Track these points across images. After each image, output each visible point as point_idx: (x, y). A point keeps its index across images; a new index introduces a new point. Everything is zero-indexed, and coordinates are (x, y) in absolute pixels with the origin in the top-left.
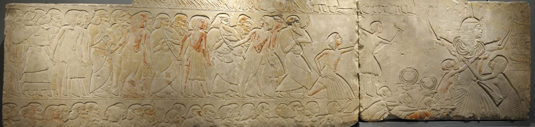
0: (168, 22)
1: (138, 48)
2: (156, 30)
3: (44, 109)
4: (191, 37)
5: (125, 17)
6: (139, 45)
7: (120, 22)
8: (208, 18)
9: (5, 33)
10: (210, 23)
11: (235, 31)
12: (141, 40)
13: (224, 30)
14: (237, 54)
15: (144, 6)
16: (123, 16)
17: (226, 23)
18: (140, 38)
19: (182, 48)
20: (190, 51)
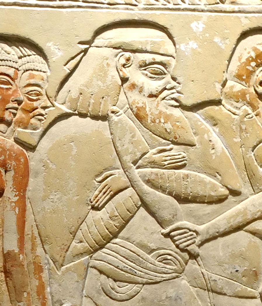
8: (45, 57)
9: (41, 57)
10: (50, 87)
11: (213, 134)
13: (140, 133)
14: (221, 282)
17: (154, 85)
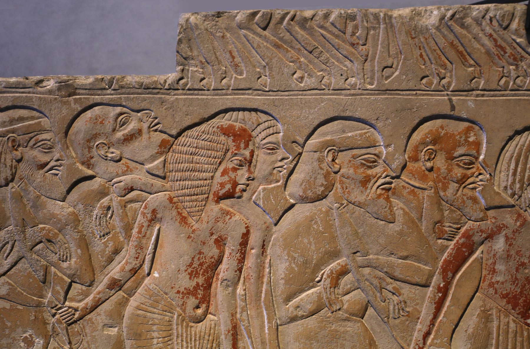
0: (371, 164)
1: (206, 299)
2: (302, 211)
3: (264, 120)
4: (500, 244)
5: (136, 144)
6: (208, 285)
7: (113, 167)
12: (219, 261)
15: (243, 78)
16: (129, 138)
18: (215, 252)
19: (439, 305)
20: (486, 317)
